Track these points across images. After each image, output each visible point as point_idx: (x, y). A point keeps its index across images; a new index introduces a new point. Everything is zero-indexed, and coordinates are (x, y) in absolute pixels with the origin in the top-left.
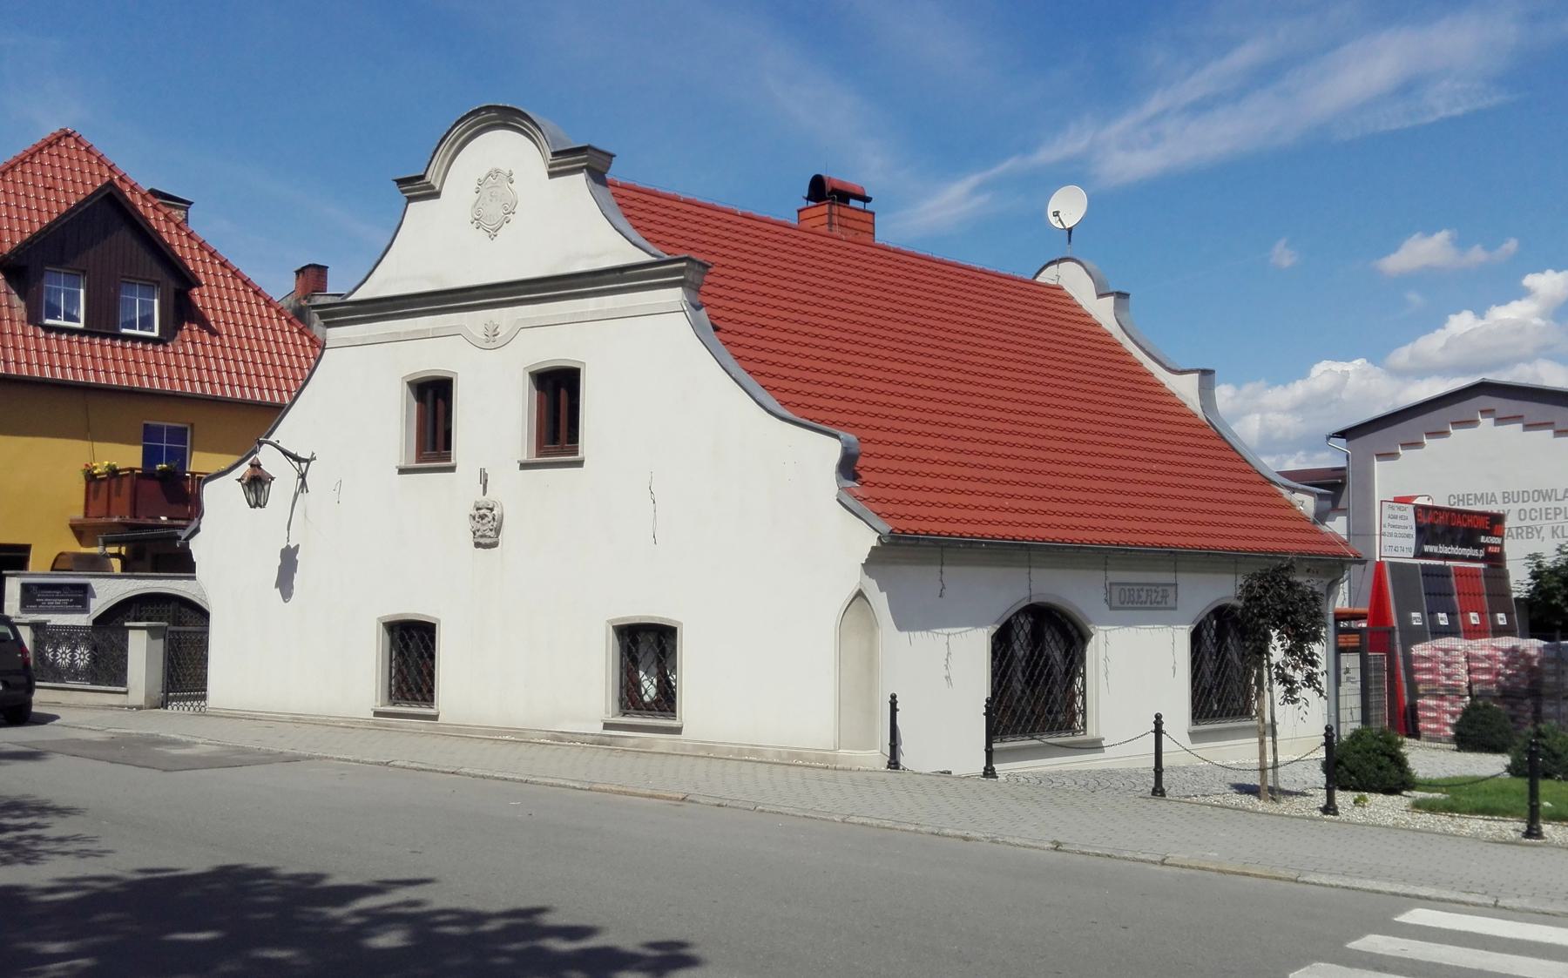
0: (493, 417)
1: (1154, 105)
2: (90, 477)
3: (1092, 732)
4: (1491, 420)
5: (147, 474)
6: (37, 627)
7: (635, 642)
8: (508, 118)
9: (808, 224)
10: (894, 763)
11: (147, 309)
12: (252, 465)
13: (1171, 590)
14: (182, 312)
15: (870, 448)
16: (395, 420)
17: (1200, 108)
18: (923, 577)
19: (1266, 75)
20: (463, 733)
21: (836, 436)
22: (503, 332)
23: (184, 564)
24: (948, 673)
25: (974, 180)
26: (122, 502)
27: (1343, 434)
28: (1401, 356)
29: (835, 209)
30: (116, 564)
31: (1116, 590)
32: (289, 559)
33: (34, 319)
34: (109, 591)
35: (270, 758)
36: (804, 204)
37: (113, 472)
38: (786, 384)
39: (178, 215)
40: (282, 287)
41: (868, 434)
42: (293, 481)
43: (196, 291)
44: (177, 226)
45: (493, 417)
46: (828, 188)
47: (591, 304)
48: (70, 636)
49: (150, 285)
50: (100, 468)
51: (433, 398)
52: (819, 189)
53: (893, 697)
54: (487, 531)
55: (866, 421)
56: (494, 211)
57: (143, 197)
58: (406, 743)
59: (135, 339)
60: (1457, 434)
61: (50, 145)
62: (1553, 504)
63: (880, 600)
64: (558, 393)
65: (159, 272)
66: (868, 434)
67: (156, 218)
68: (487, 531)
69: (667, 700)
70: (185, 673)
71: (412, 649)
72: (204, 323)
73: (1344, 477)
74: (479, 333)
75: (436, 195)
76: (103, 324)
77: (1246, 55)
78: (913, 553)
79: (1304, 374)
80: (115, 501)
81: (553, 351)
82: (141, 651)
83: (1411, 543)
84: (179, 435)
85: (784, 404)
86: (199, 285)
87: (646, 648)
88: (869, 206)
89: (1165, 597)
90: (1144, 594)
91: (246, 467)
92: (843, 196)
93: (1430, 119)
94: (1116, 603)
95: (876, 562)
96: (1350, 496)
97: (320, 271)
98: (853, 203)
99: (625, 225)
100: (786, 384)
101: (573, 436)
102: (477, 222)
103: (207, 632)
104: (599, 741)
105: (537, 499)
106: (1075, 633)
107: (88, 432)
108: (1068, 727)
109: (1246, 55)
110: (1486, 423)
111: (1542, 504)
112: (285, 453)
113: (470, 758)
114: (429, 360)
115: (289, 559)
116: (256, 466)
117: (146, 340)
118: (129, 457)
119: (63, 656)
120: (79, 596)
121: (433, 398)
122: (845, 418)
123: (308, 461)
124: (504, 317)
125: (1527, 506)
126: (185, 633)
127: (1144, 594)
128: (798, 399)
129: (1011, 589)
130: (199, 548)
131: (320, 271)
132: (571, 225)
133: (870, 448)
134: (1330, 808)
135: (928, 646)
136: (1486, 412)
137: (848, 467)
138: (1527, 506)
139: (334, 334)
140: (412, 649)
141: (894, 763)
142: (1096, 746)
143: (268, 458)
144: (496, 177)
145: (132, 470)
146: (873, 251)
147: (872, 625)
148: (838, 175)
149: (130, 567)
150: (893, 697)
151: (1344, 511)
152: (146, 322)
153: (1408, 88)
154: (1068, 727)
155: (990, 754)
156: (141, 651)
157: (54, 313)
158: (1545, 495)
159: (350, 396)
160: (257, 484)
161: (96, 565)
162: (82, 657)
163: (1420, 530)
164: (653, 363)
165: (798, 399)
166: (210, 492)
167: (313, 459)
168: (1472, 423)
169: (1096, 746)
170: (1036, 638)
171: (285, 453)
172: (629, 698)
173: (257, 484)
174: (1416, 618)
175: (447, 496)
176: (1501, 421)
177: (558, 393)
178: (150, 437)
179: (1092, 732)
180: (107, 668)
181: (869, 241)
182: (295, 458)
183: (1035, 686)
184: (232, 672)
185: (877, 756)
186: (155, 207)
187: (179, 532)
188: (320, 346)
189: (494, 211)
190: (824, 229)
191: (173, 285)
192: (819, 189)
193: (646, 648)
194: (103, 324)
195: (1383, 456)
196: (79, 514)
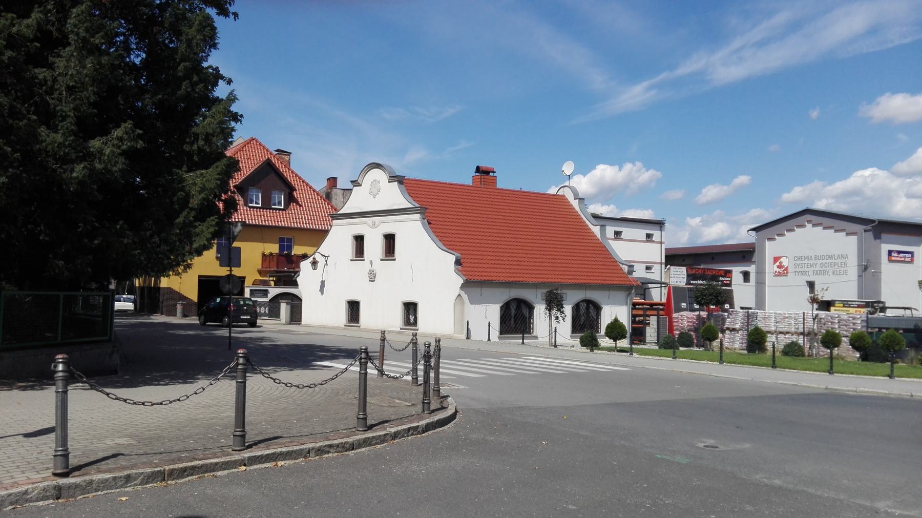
0: (374, 246)
1: (737, 43)
2: (264, 255)
3: (535, 334)
4: (811, 225)
5: (280, 255)
8: (378, 166)
10: (468, 338)
11: (279, 198)
14: (291, 199)
16: (349, 247)
17: (762, 44)
18: (476, 291)
19: (794, 27)
20: (366, 330)
23: (295, 284)
24: (487, 315)
25: (646, 84)
26: (274, 263)
28: (902, 166)
30: (272, 283)
32: (323, 283)
33: (246, 204)
34: (274, 291)
35: (315, 334)
37: (271, 254)
39: (287, 158)
40: (320, 185)
42: (324, 263)
47: (398, 217)
48: (262, 304)
49: (280, 190)
50: (267, 252)
51: (359, 240)
58: (353, 332)
59: (276, 209)
60: (798, 230)
62: (833, 261)
63: (465, 297)
64: (390, 239)
65: (283, 187)
69: (415, 323)
70: (296, 316)
71: (354, 307)
72: (297, 203)
73: (754, 249)
74: (371, 224)
76: (267, 205)
77: (782, 18)
78: (475, 283)
79: (846, 175)
80: (272, 263)
81: (389, 230)
82: (284, 308)
83: (685, 280)
84: (290, 240)
87: (410, 308)
93: (890, 45)
95: (463, 287)
96: (756, 257)
97: (335, 179)
99: (407, 195)
104: (399, 333)
105: (384, 268)
107: (263, 240)
108: (530, 333)
109: (782, 18)
110: (809, 226)
111: (829, 261)
113: (365, 335)
114: (358, 231)
115: (323, 283)
117: (280, 209)
118: (274, 248)
119: (263, 310)
120: (265, 293)
121: (359, 240)
124: (377, 219)
125: (824, 262)
126: (295, 303)
129: (507, 294)
130: (299, 280)
131: (335, 179)
132: (394, 197)
135: (480, 309)
136: (809, 222)
137: (458, 262)
138: (824, 262)
140: (354, 307)
141: (468, 338)
142: (536, 337)
143: (318, 257)
147: (463, 303)
148: (484, 164)
149: (277, 284)
151: (754, 263)
152: (280, 204)
153: (873, 31)
154: (530, 333)
156: (284, 308)
157: (252, 202)
158: (830, 257)
159: (340, 236)
163: (688, 276)
164: (412, 233)
168: (803, 226)
169: (536, 337)
172: (407, 322)
173: (314, 263)
174: (684, 305)
175: (362, 267)
176: (814, 225)
177: (390, 239)
178: (281, 240)
179: (535, 334)
180: (274, 313)
183: (516, 320)
184: (308, 315)
185: (464, 336)
191: (288, 191)
193: (410, 308)
194: (267, 205)
195: (769, 239)
196: (260, 267)
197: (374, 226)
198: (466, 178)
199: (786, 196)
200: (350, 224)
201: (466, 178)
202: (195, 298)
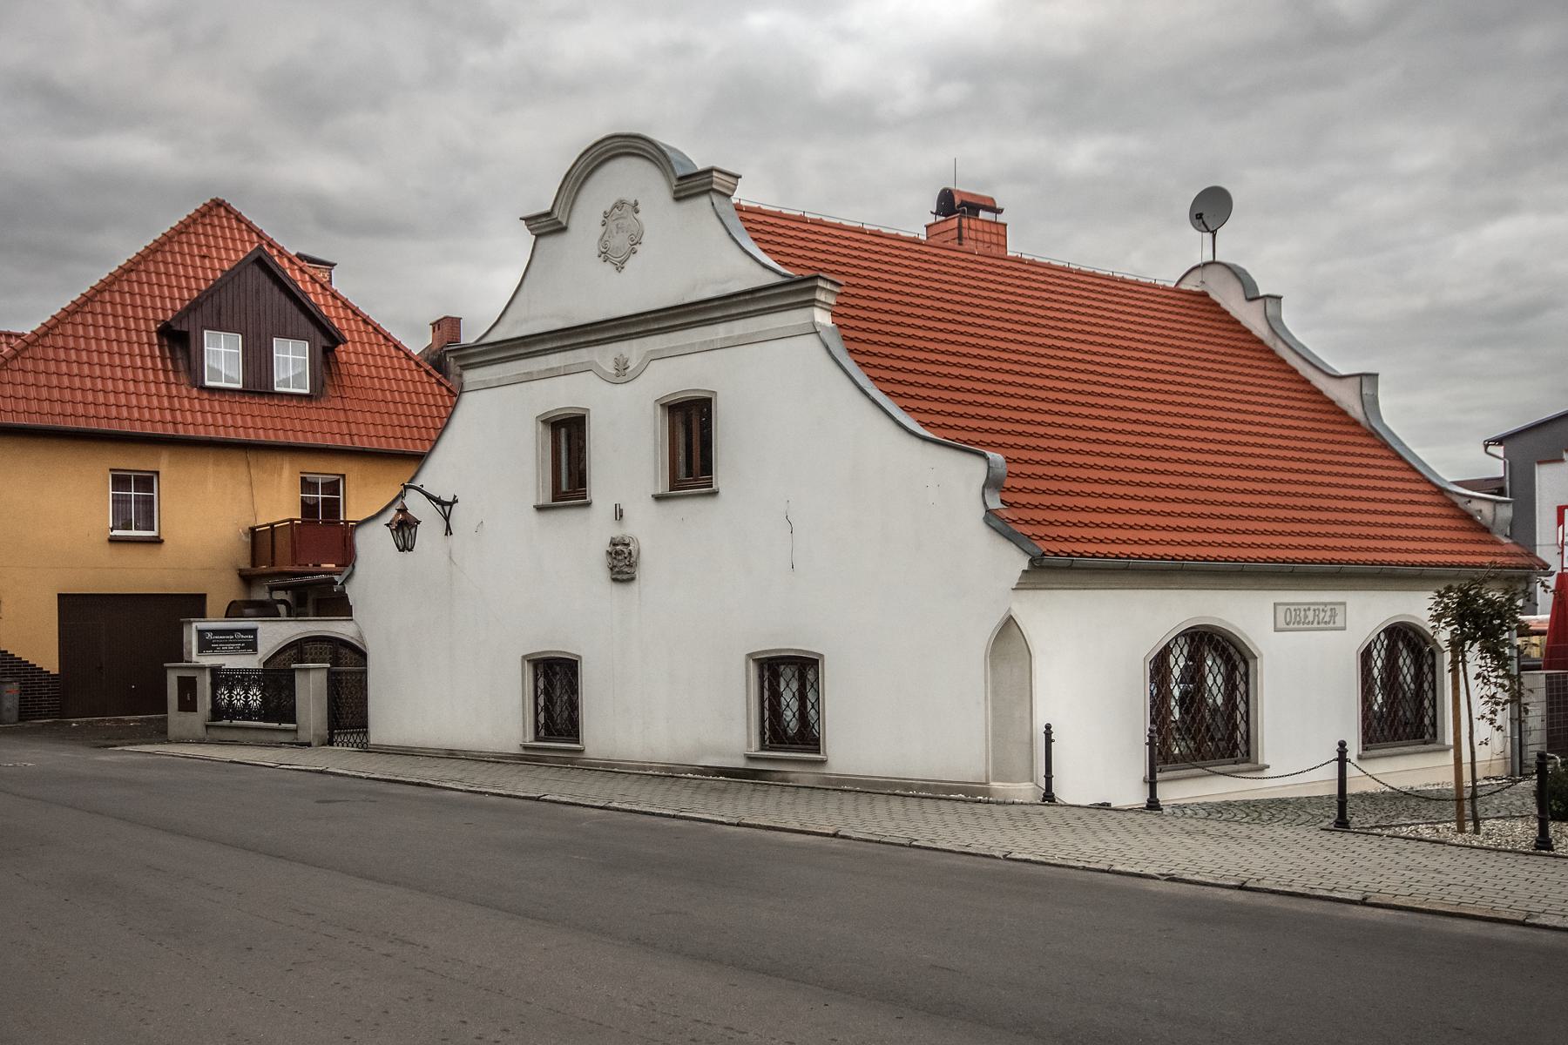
0: (627, 452)
6: (215, 671)
7: (775, 676)
9: (936, 241)
12: (399, 511)
13: (1339, 609)
15: (1016, 468)
16: (528, 466)
20: (611, 769)
21: (983, 455)
22: (632, 365)
23: (339, 606)
27: (1499, 441)
29: (965, 222)
30: (282, 608)
31: (1281, 610)
34: (274, 634)
36: (931, 220)
38: (925, 405)
41: (1014, 454)
43: (341, 347)
44: (322, 286)
45: (627, 452)
46: (957, 201)
51: (568, 434)
52: (948, 204)
53: (1048, 727)
54: (622, 564)
55: (1011, 440)
56: (619, 241)
57: (290, 260)
61: (204, 215)
65: (311, 328)
66: (1014, 454)
67: (303, 284)
68: (622, 564)
70: (348, 714)
71: (556, 679)
74: (610, 368)
75: (564, 229)
82: (311, 688)
85: (925, 425)
86: (345, 342)
88: (1001, 218)
89: (1333, 616)
90: (1311, 614)
91: (392, 513)
92: (973, 207)
94: (1282, 624)
98: (983, 215)
100: (925, 405)
101: (707, 468)
102: (605, 255)
103: (365, 672)
105: (659, 530)
106: (1237, 657)
112: (430, 497)
114: (561, 395)
115: (1561, 521)
116: (403, 510)
121: (568, 434)
122: (988, 438)
123: (450, 504)
126: (348, 670)
127: (1311, 614)
128: (938, 420)
130: (353, 592)
133: (1016, 468)
134: (1543, 843)
139: (471, 376)
140: (556, 679)
143: (416, 504)
144: (624, 208)
145: (292, 520)
146: (1007, 264)
148: (966, 186)
149: (297, 610)
150: (1048, 727)
155: (1152, 783)
156: (311, 688)
160: (405, 528)
161: (267, 610)
162: (255, 697)
165: (938, 420)
166: (362, 539)
167: (455, 501)
170: (1195, 658)
171: (430, 497)
173: (405, 528)
175: (588, 532)
181: (1001, 254)
182: (438, 501)
186: (301, 270)
187: (336, 578)
188: (455, 394)
189: (619, 241)
190: (955, 244)
192: (948, 204)
196: (245, 564)
197: (622, 372)
198: (911, 217)
199: (7, 704)
200: (529, 378)
201: (911, 217)
202: (49, 661)
